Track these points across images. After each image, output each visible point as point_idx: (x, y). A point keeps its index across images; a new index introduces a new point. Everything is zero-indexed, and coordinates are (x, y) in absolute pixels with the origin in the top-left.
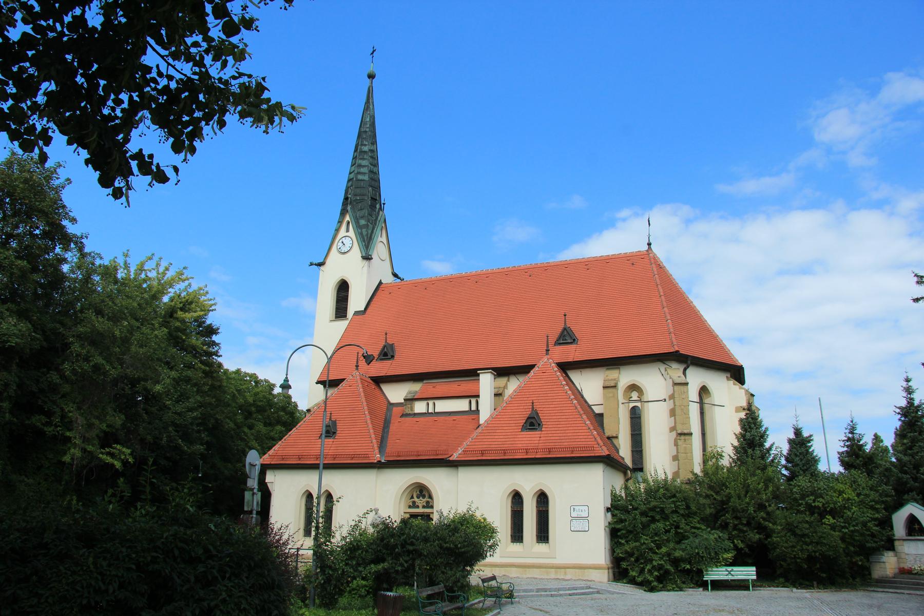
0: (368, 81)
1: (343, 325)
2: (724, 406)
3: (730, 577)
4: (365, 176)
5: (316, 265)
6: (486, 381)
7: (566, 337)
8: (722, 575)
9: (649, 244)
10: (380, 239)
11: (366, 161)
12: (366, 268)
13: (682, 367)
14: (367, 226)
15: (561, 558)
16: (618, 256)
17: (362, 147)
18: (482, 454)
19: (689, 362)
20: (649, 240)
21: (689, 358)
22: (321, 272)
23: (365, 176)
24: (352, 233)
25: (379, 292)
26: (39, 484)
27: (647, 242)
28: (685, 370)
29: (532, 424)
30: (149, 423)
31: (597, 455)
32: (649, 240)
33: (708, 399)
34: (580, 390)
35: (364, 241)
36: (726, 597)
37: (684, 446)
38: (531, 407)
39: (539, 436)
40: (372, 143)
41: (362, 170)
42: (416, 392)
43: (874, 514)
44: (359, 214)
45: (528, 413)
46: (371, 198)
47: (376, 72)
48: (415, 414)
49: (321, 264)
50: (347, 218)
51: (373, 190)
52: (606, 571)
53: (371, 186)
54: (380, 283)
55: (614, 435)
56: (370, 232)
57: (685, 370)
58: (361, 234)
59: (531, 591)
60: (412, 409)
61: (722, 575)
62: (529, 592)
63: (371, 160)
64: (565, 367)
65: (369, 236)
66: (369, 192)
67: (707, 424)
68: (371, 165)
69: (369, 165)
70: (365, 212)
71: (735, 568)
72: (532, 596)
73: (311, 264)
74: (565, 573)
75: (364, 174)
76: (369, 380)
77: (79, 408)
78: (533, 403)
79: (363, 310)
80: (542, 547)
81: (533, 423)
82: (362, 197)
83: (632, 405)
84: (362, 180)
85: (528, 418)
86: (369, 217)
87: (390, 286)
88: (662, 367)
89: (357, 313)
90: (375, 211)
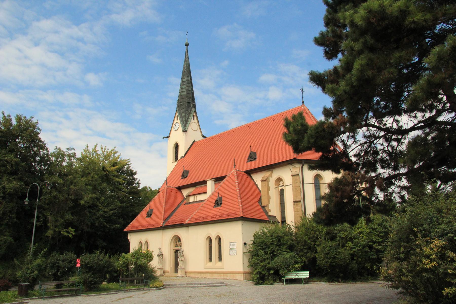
0: (186, 47)
1: (176, 163)
3: (297, 277)
5: (166, 138)
6: (210, 185)
7: (252, 157)
8: (293, 276)
9: (303, 102)
10: (192, 121)
11: (185, 85)
12: (184, 136)
13: (300, 166)
14: (185, 116)
16: (289, 111)
18: (196, 220)
19: (303, 163)
20: (303, 100)
21: (303, 161)
22: (168, 141)
24: (179, 121)
25: (193, 146)
26: (41, 245)
27: (302, 101)
28: (302, 167)
29: (218, 204)
30: (90, 217)
31: (238, 217)
32: (303, 100)
33: (322, 181)
35: (184, 123)
37: (297, 208)
38: (217, 196)
39: (219, 209)
40: (187, 77)
41: (183, 90)
42: (191, 192)
43: (379, 239)
44: (182, 111)
45: (216, 198)
46: (188, 102)
47: (189, 42)
48: (190, 203)
49: (168, 137)
50: (177, 114)
51: (188, 98)
52: (243, 275)
53: (187, 97)
54: (194, 141)
55: (266, 205)
56: (187, 118)
57: (302, 167)
58: (183, 120)
59: (183, 284)
60: (189, 200)
61: (293, 276)
62: (183, 285)
63: (187, 85)
64: (249, 173)
66: (186, 100)
68: (188, 87)
69: (186, 87)
70: (184, 110)
71: (300, 272)
72: (184, 287)
73: (164, 138)
75: (184, 91)
76: (176, 189)
77: (51, 214)
78: (218, 193)
79: (184, 155)
80: (220, 263)
81: (218, 203)
82: (183, 103)
83: (280, 188)
84: (183, 95)
85: (216, 201)
87: (200, 142)
88: (291, 167)
89: (182, 157)
90: (190, 108)
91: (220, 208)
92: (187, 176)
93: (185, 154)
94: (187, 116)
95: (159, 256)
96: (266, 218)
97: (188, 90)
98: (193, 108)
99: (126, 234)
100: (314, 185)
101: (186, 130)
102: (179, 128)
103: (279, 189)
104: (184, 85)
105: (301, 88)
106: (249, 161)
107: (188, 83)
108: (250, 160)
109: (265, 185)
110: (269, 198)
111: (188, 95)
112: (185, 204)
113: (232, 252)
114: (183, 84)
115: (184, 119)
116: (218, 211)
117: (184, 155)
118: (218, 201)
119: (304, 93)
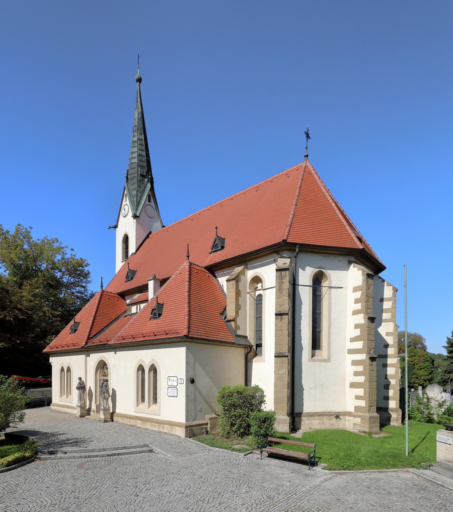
2: (342, 288)
4: (135, 159)
5: (113, 227)
15: (163, 417)
17: (134, 138)
23: (135, 159)
24: (128, 202)
34: (222, 285)
35: (134, 206)
36: (293, 471)
38: (156, 301)
40: (140, 134)
49: (116, 227)
50: (126, 192)
53: (140, 166)
56: (139, 199)
60: (130, 311)
65: (138, 202)
67: (324, 305)
73: (110, 228)
74: (163, 427)
76: (118, 296)
83: (258, 293)
85: (153, 310)
86: (139, 188)
90: (144, 184)
91: (157, 320)
92: (132, 278)
93: (137, 251)
94: (140, 195)
95: (78, 388)
96: (232, 339)
97: (140, 155)
98: (148, 184)
99: (47, 356)
100: (312, 288)
101: (138, 215)
102: (128, 212)
103: (255, 295)
104: (135, 147)
105: (306, 130)
106: (214, 252)
107: (140, 144)
108: (214, 250)
109: (233, 288)
110: (238, 308)
111: (142, 164)
112: (125, 317)
113: (172, 392)
114: (133, 146)
115: (135, 199)
116: (154, 325)
117: (135, 251)
118: (155, 309)
119: (309, 140)
